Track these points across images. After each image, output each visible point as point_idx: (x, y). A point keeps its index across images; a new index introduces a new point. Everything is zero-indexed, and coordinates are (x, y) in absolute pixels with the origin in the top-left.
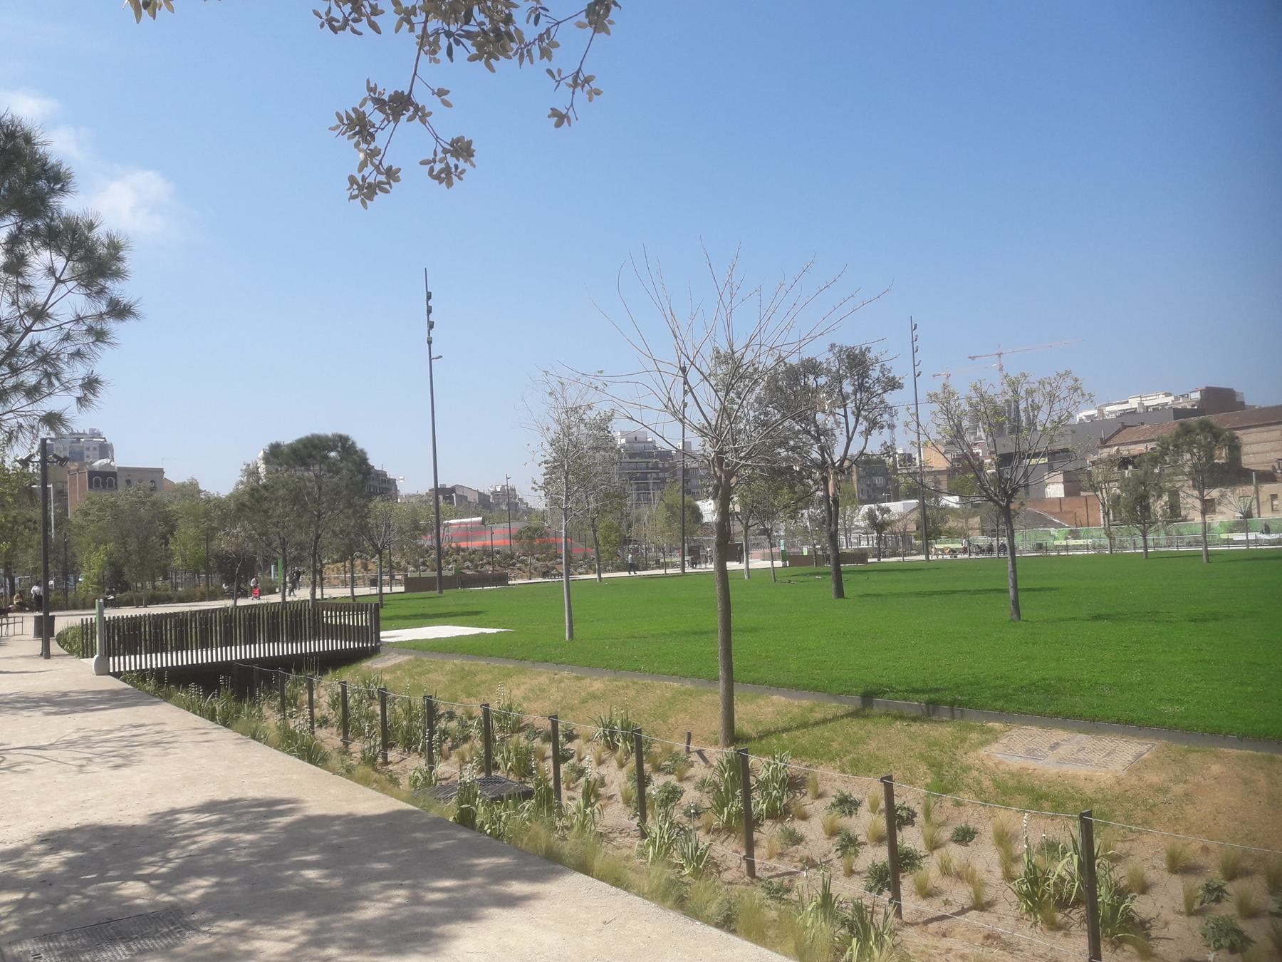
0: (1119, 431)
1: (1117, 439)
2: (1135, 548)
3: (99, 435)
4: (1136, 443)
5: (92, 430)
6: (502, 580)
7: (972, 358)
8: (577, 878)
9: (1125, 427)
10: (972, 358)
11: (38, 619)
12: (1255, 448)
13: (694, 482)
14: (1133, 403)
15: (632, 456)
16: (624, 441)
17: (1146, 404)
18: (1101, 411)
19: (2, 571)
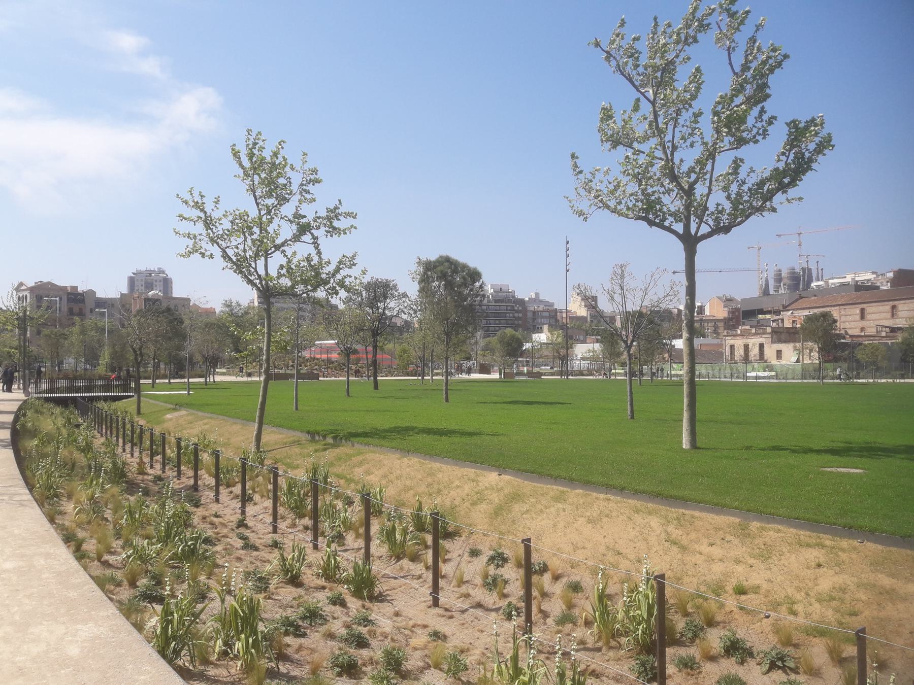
0: (797, 300)
1: (793, 306)
2: (732, 376)
3: (163, 272)
4: (804, 309)
5: (159, 269)
6: (316, 377)
7: (779, 236)
8: (780, 671)
9: (801, 298)
10: (779, 236)
11: (586, 318)
12: (873, 316)
13: (539, 320)
14: (849, 279)
15: (496, 301)
16: (492, 291)
17: (857, 279)
18: (826, 283)
19: (6, 434)
